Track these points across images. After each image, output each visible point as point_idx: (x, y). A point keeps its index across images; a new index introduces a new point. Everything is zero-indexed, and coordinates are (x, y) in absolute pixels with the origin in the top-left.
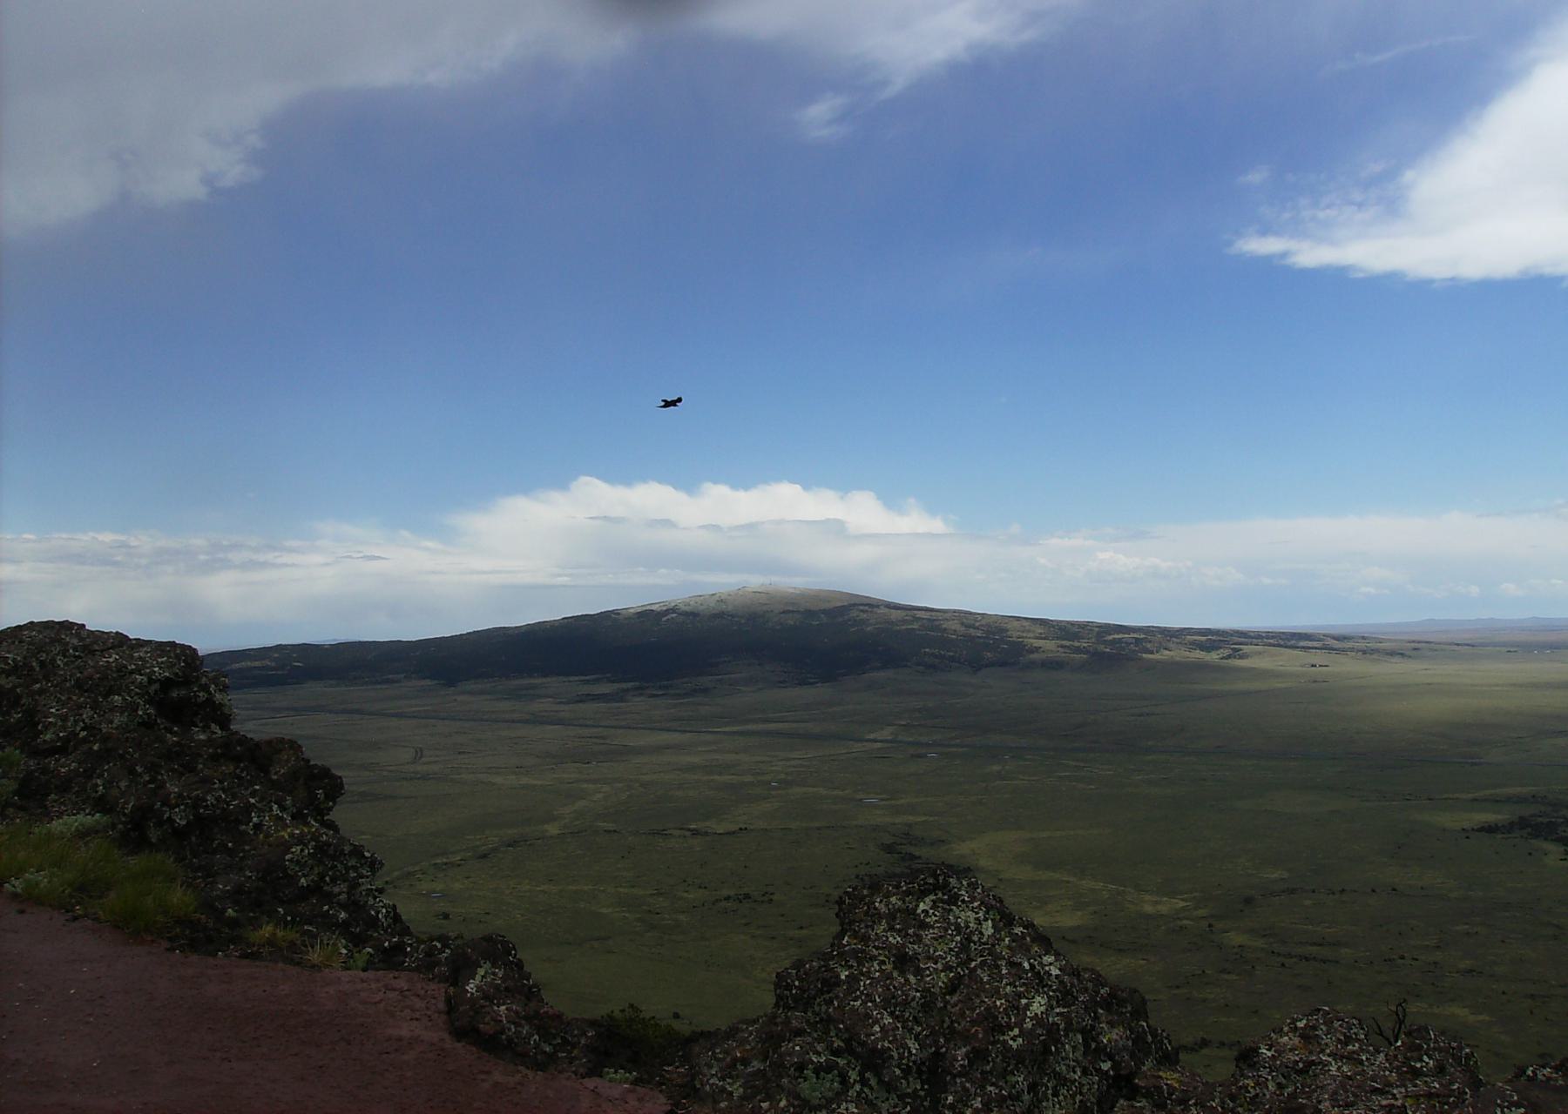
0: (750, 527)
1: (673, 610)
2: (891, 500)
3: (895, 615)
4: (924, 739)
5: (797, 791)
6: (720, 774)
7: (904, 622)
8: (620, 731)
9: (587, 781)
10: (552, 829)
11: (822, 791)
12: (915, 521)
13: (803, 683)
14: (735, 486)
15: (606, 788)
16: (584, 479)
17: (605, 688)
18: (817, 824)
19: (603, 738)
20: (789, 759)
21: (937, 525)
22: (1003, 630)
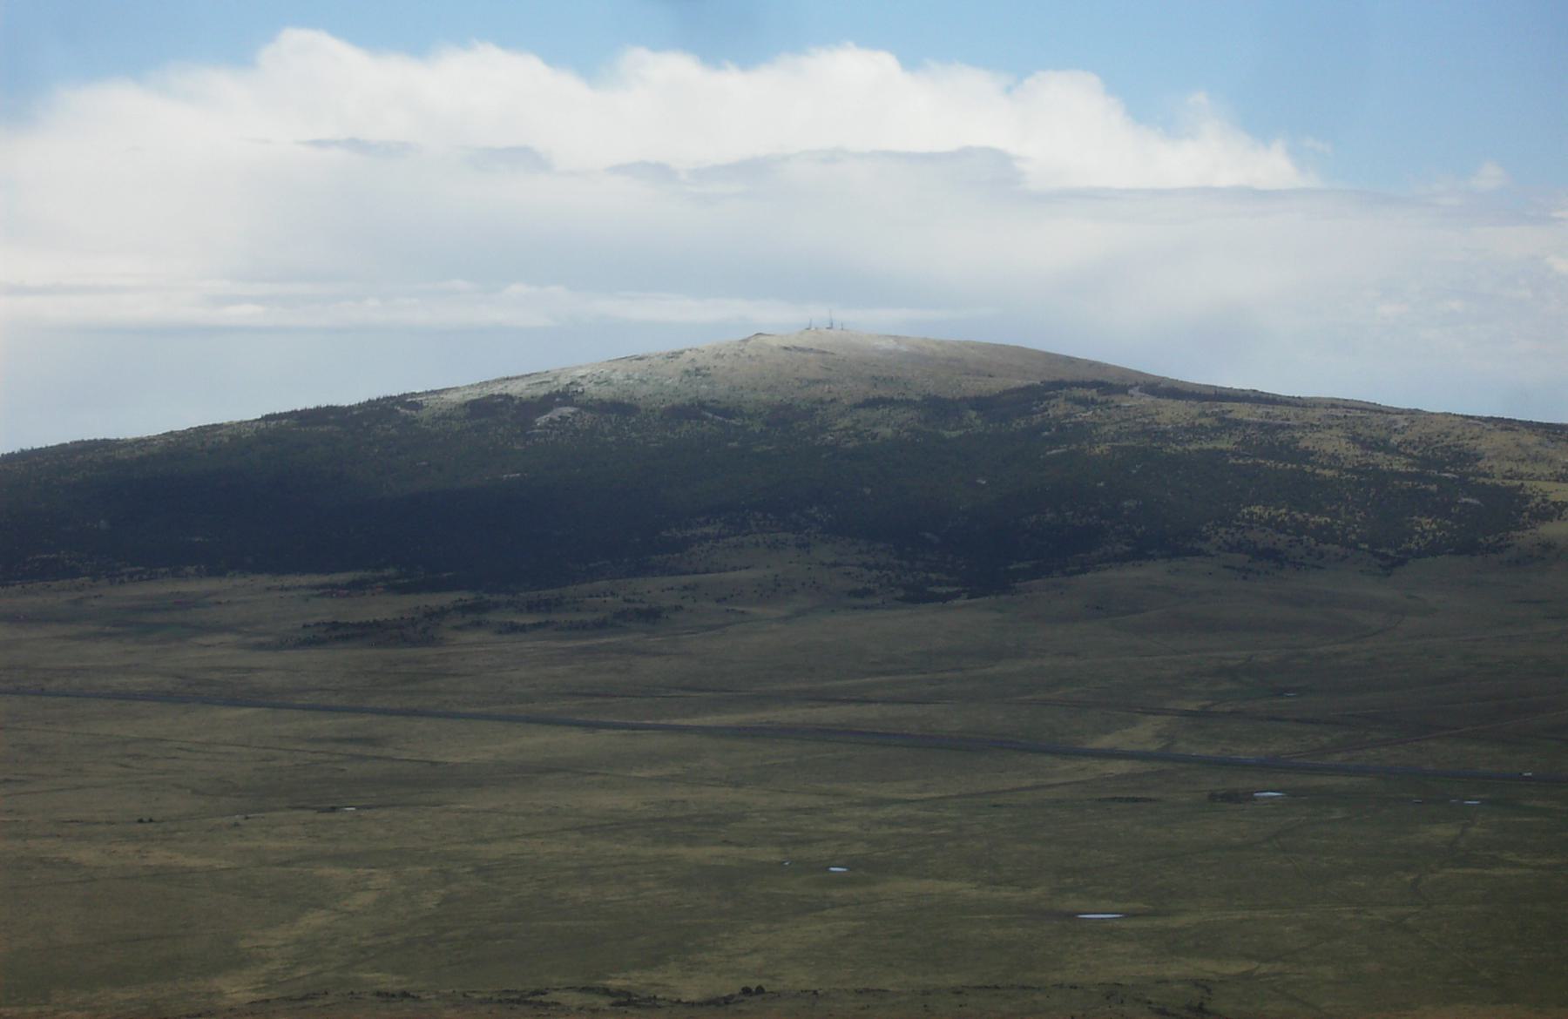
0: (753, 169)
1: (565, 396)
2: (1146, 101)
3: (1172, 413)
4: (1246, 752)
5: (900, 889)
6: (691, 841)
7: (1195, 431)
8: (421, 724)
9: (338, 859)
10: (236, 990)
11: (965, 889)
12: (1208, 157)
13: (917, 596)
14: (911, 61)
15: (383, 879)
16: (294, 38)
17: (382, 608)
18: (954, 980)
19: (371, 741)
20: (878, 803)
21: (1272, 167)
22: (1464, 457)
